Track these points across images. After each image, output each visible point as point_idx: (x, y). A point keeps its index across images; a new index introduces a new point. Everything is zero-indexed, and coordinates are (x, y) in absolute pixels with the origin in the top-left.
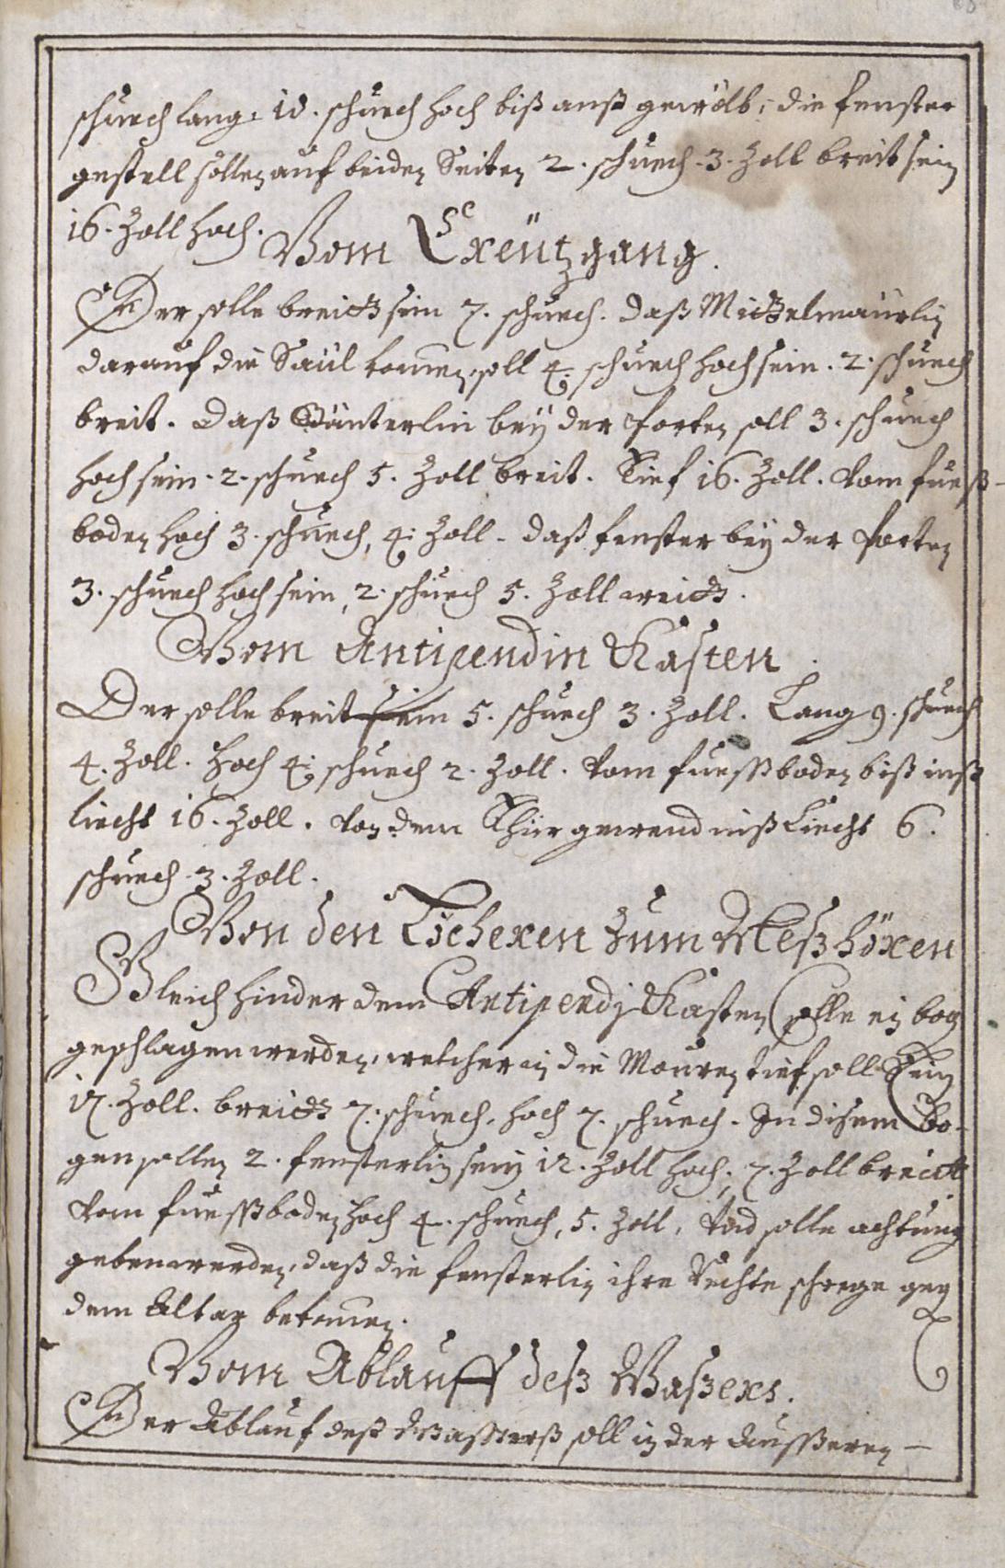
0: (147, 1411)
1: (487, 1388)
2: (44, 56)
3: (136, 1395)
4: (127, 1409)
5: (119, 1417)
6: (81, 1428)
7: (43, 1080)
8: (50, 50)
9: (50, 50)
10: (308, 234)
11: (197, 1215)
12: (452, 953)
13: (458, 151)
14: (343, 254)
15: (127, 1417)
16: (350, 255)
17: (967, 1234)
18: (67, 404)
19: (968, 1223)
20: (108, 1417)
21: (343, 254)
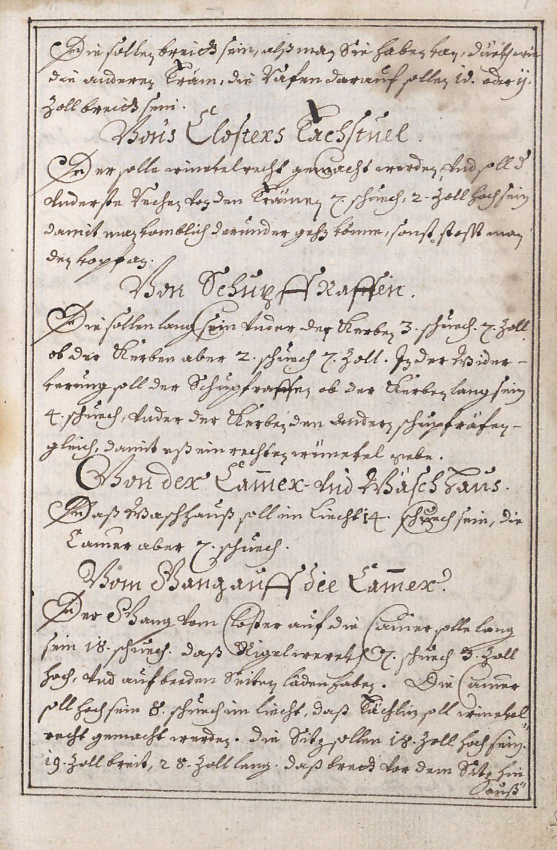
0: (84, 611)
1: (286, 591)
2: (32, 31)
3: (78, 601)
4: (75, 607)
5: (71, 611)
6: (56, 518)
7: (32, 345)
8: (35, 27)
9: (35, 27)
10: (150, 280)
11: (109, 547)
12: (330, 145)
13: (202, 378)
14: (137, 483)
15: (75, 612)
16: (141, 485)
17: (533, 709)
18: (42, 252)
19: (533, 705)
20: (65, 611)
21: (137, 483)
